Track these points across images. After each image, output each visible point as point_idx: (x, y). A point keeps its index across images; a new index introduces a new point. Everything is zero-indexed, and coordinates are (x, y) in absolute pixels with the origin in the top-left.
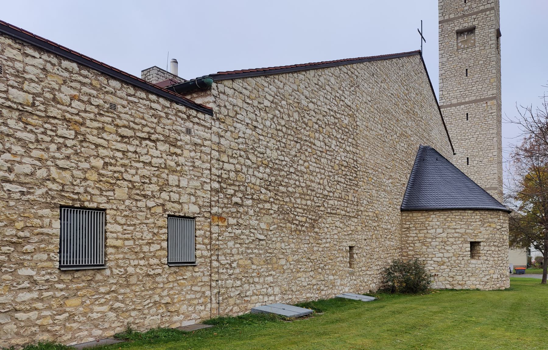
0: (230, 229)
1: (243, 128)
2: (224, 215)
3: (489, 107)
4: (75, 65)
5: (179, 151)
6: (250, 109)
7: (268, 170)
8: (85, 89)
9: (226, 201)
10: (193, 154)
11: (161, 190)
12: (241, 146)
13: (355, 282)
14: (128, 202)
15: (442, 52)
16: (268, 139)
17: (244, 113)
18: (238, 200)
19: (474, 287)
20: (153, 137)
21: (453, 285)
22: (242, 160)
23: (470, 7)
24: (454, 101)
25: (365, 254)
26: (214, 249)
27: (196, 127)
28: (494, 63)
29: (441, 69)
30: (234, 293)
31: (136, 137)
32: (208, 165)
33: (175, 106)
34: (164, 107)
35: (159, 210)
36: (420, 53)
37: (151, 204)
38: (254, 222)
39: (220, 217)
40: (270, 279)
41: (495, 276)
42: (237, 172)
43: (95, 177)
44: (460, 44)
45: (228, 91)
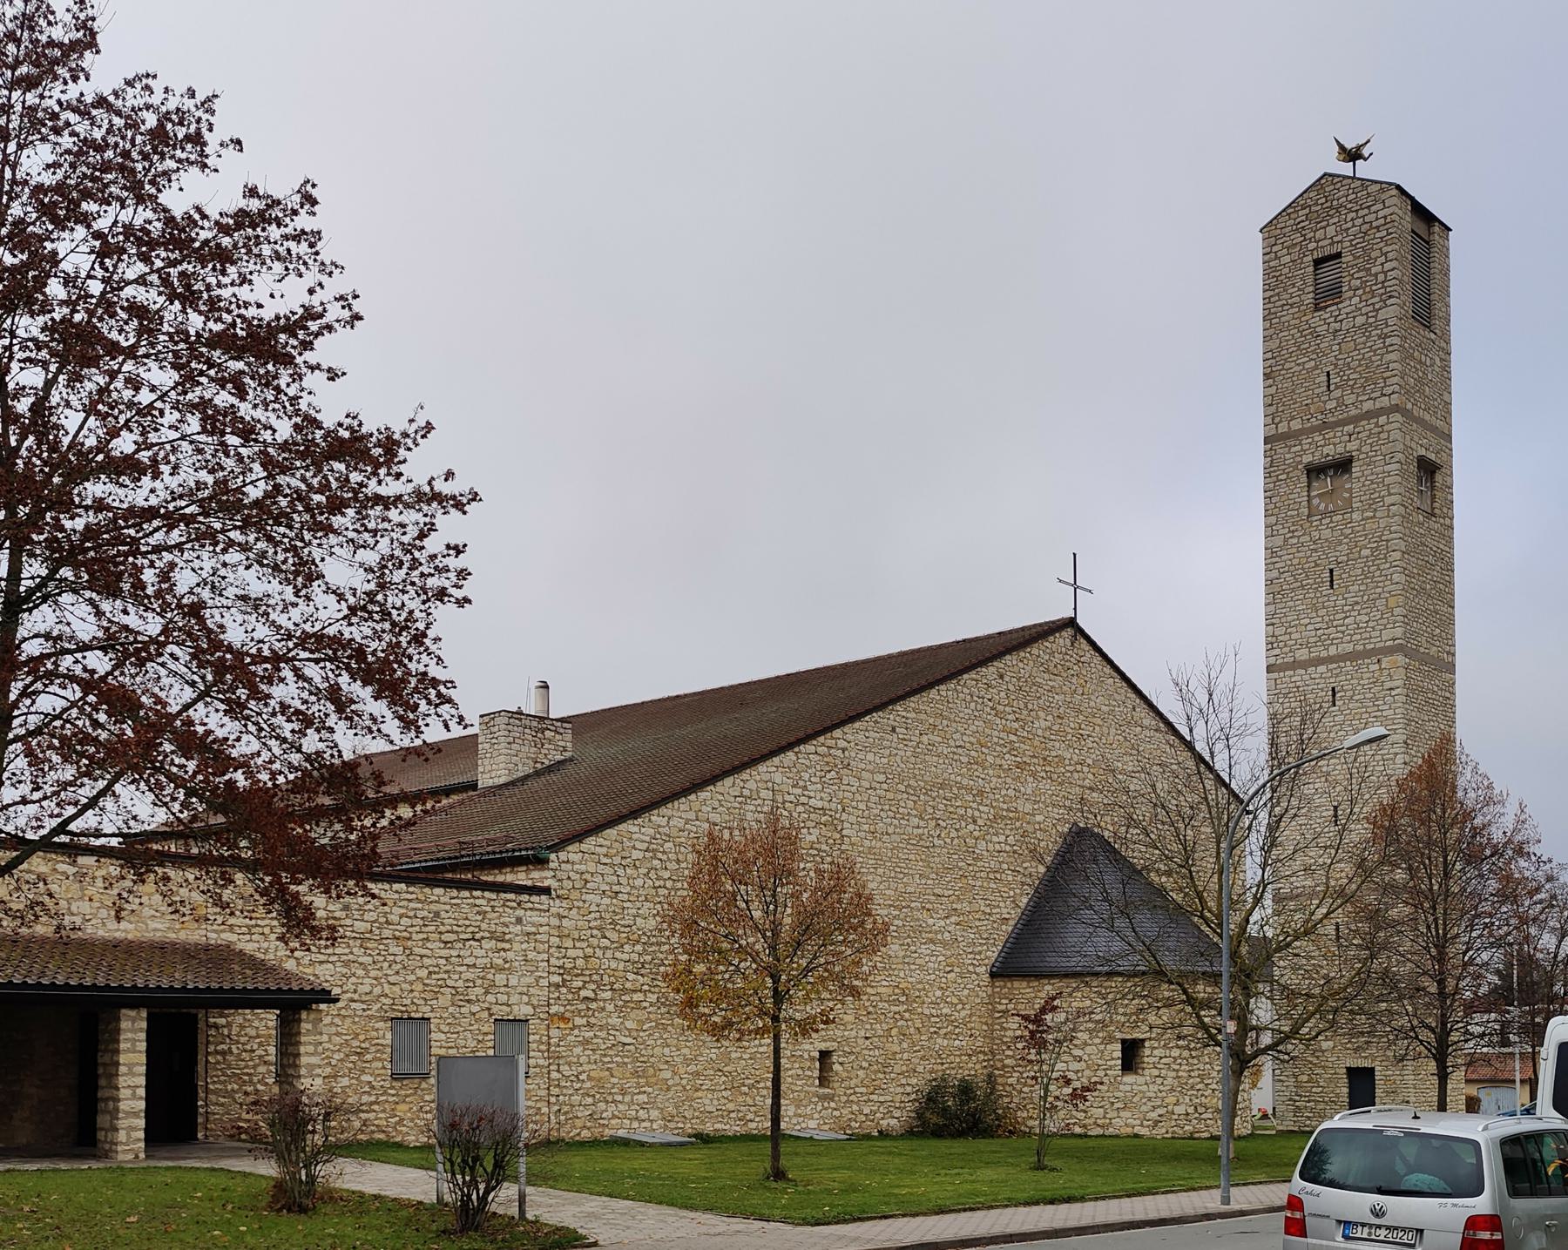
0: (576, 1032)
1: (597, 899)
2: (567, 1015)
3: (1386, 672)
4: (403, 886)
5: (507, 946)
6: (608, 870)
7: (639, 948)
8: (412, 905)
9: (570, 997)
10: (525, 946)
11: (487, 993)
12: (593, 924)
13: (836, 1113)
14: (451, 1010)
15: (1273, 519)
16: (638, 905)
17: (599, 879)
18: (591, 994)
19: (1129, 1130)
20: (478, 936)
21: (1085, 1126)
22: (594, 942)
23: (1340, 402)
24: (1302, 655)
25: (865, 1064)
26: (554, 1057)
27: (529, 913)
28: (1397, 555)
29: (1269, 566)
30: (584, 1113)
31: (459, 940)
32: (545, 956)
33: (503, 895)
34: (490, 900)
35: (485, 1014)
36: (1071, 623)
37: (475, 1009)
38: (614, 1021)
39: (562, 1018)
40: (644, 1098)
41: (1180, 1110)
42: (586, 957)
43: (420, 987)
44: (1315, 501)
45: (572, 857)
